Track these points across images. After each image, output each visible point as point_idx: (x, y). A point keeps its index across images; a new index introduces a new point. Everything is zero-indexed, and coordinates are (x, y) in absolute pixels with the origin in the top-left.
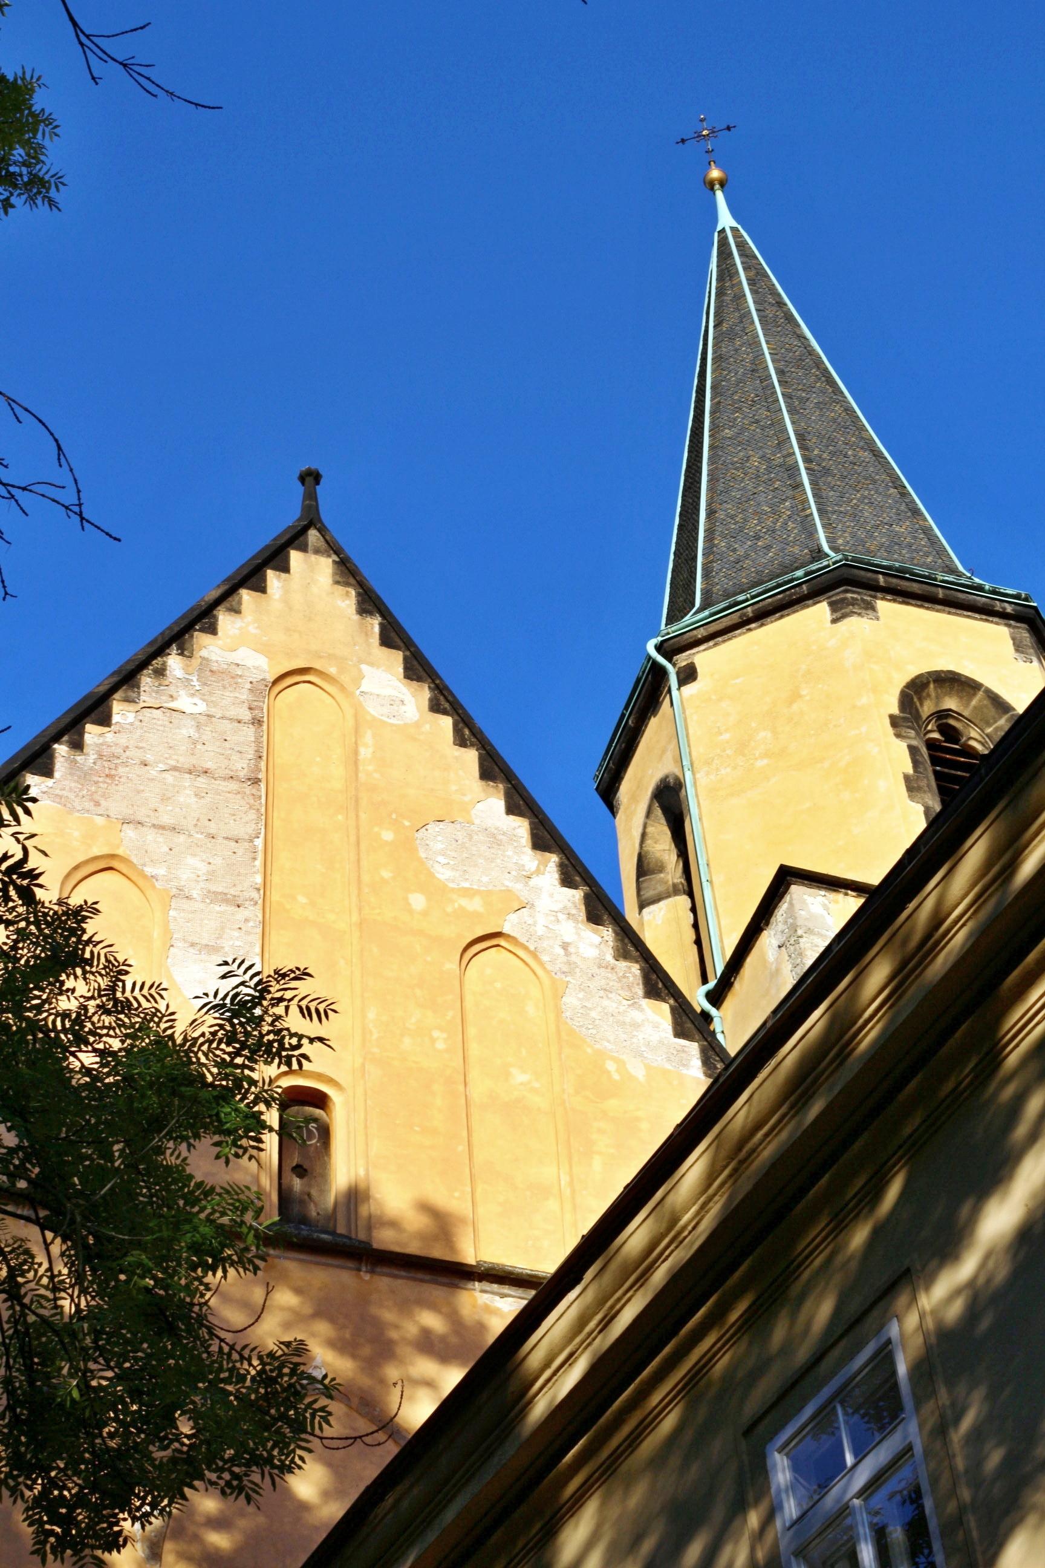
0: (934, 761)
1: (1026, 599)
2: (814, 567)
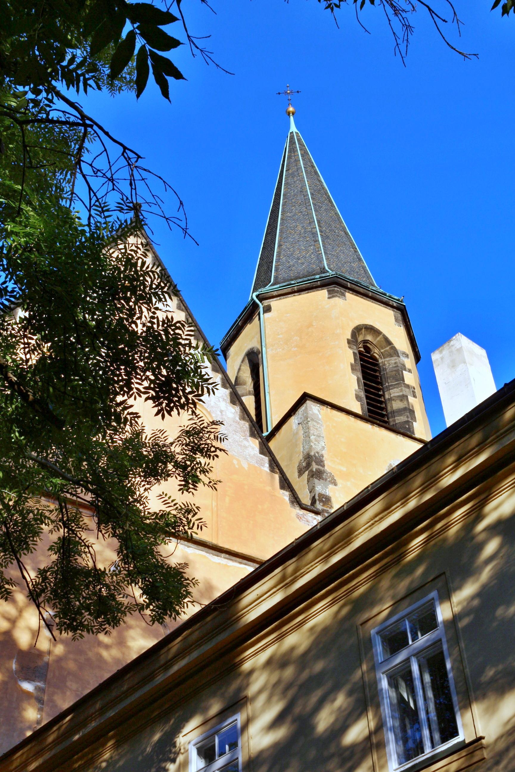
0: (361, 360)
1: (401, 302)
2: (323, 275)
